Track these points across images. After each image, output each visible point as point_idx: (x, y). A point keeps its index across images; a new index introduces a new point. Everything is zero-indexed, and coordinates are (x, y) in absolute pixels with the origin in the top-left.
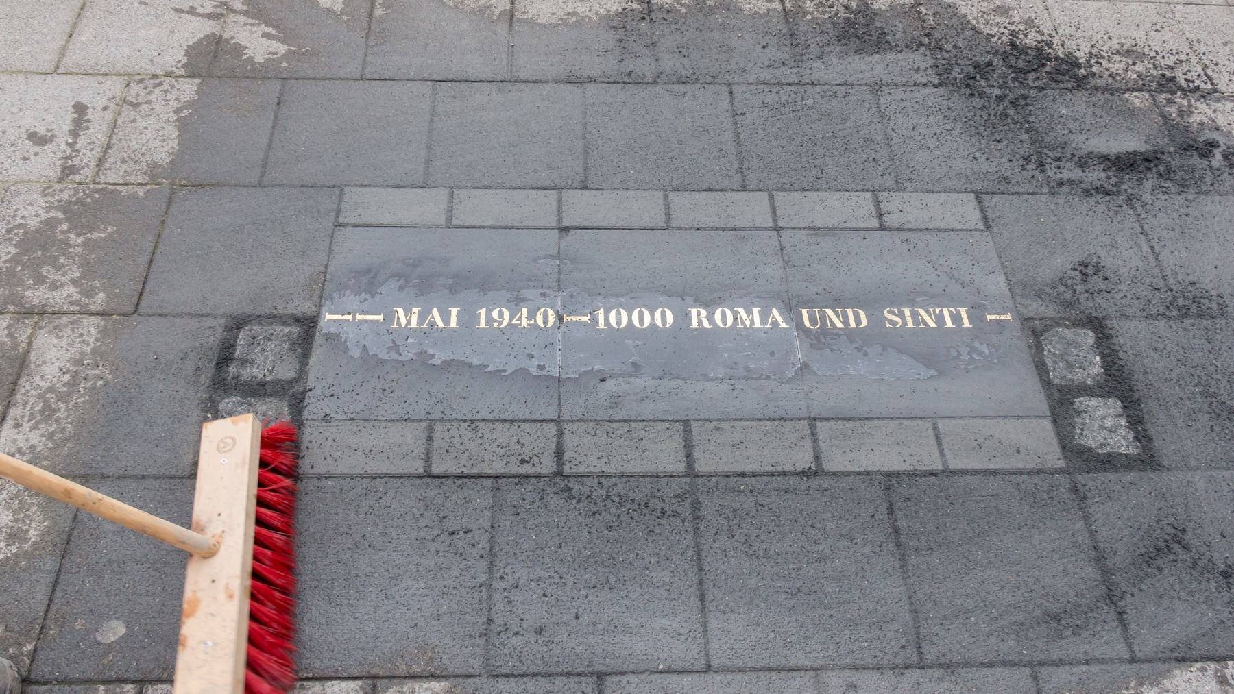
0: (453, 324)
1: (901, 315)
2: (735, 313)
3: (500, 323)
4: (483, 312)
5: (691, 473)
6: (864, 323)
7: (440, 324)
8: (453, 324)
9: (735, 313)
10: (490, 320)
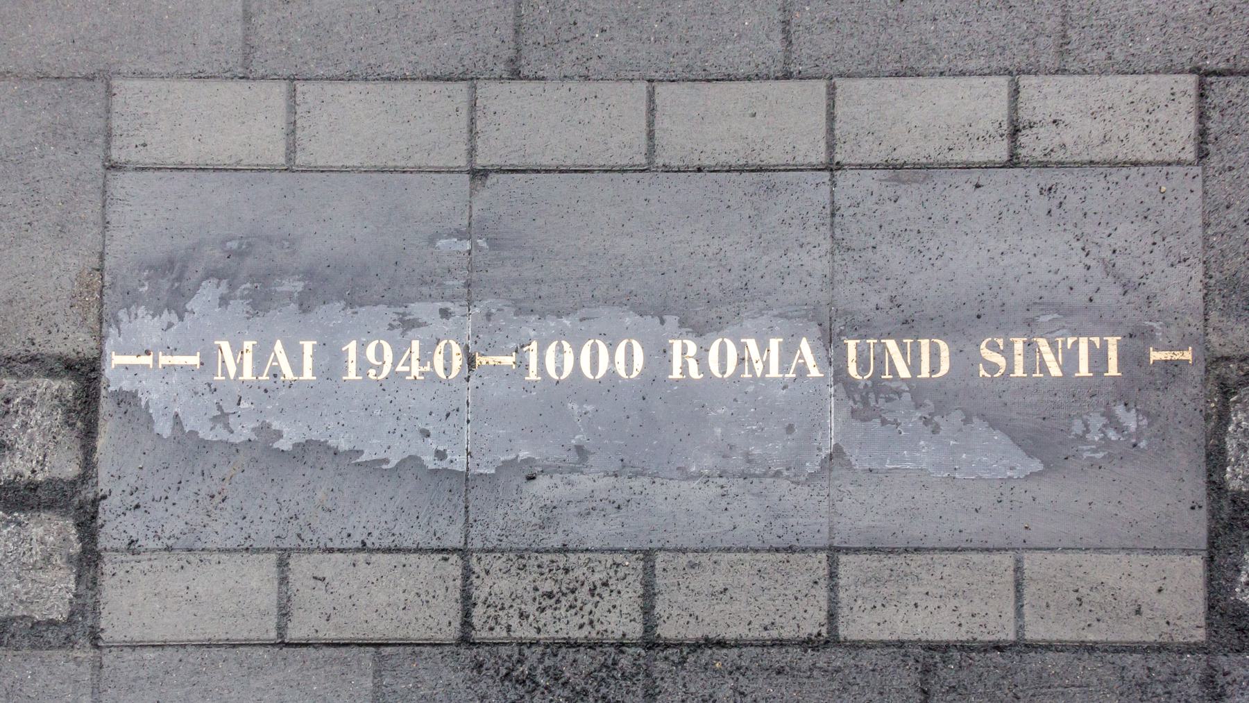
1: (1008, 352)
2: (741, 347)
3: (379, 369)
9: (741, 347)
10: (363, 366)
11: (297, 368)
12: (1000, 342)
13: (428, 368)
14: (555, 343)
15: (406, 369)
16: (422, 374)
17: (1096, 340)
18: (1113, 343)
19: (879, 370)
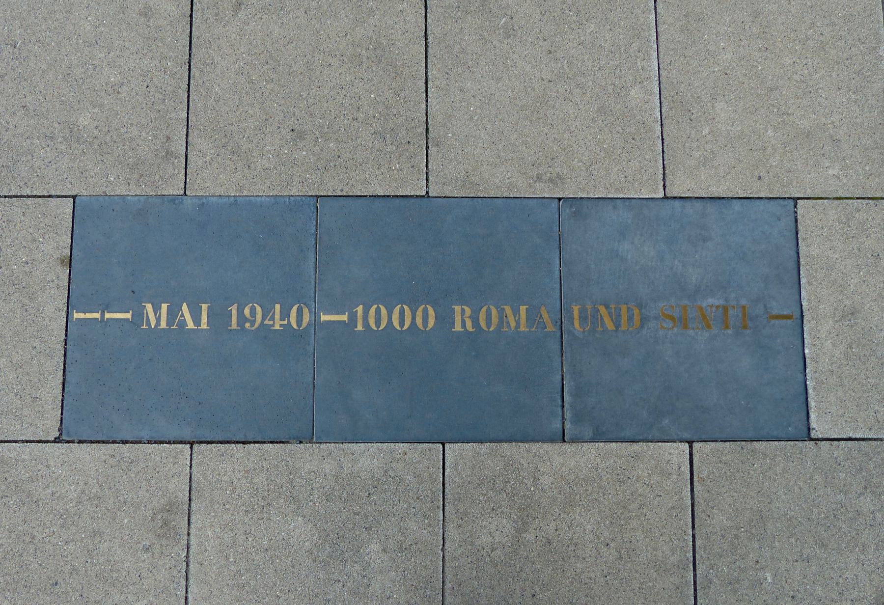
0: (204, 326)
2: (501, 312)
3: (253, 323)
4: (234, 309)
5: (690, 443)
6: (431, 322)
7: (191, 325)
8: (204, 326)
9: (501, 312)
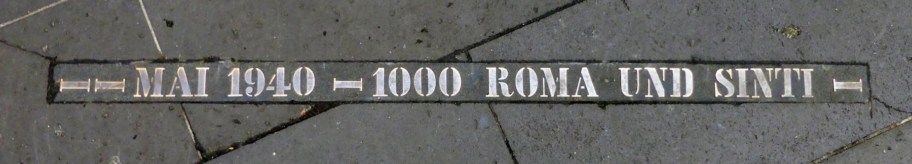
1: (735, 80)
2: (541, 75)
3: (255, 87)
9: (541, 75)
10: (243, 86)
11: (194, 88)
12: (730, 71)
13: (289, 88)
14: (420, 69)
15: (272, 88)
16: (286, 92)
17: (797, 70)
18: (808, 72)
19: (644, 90)
